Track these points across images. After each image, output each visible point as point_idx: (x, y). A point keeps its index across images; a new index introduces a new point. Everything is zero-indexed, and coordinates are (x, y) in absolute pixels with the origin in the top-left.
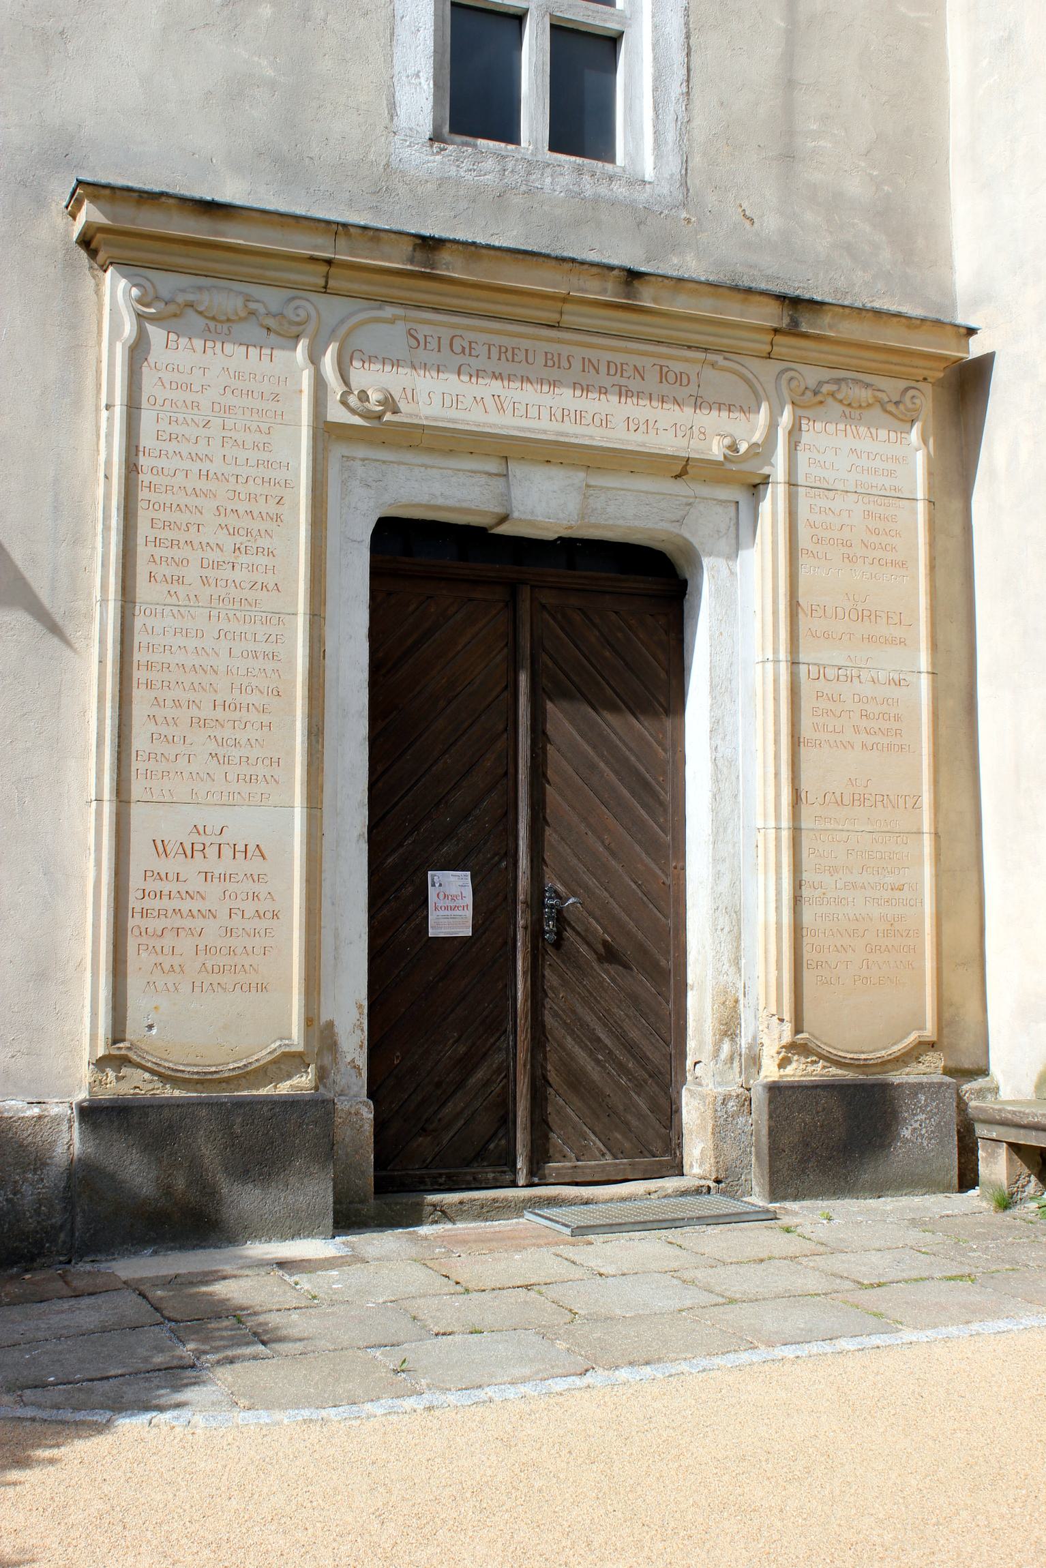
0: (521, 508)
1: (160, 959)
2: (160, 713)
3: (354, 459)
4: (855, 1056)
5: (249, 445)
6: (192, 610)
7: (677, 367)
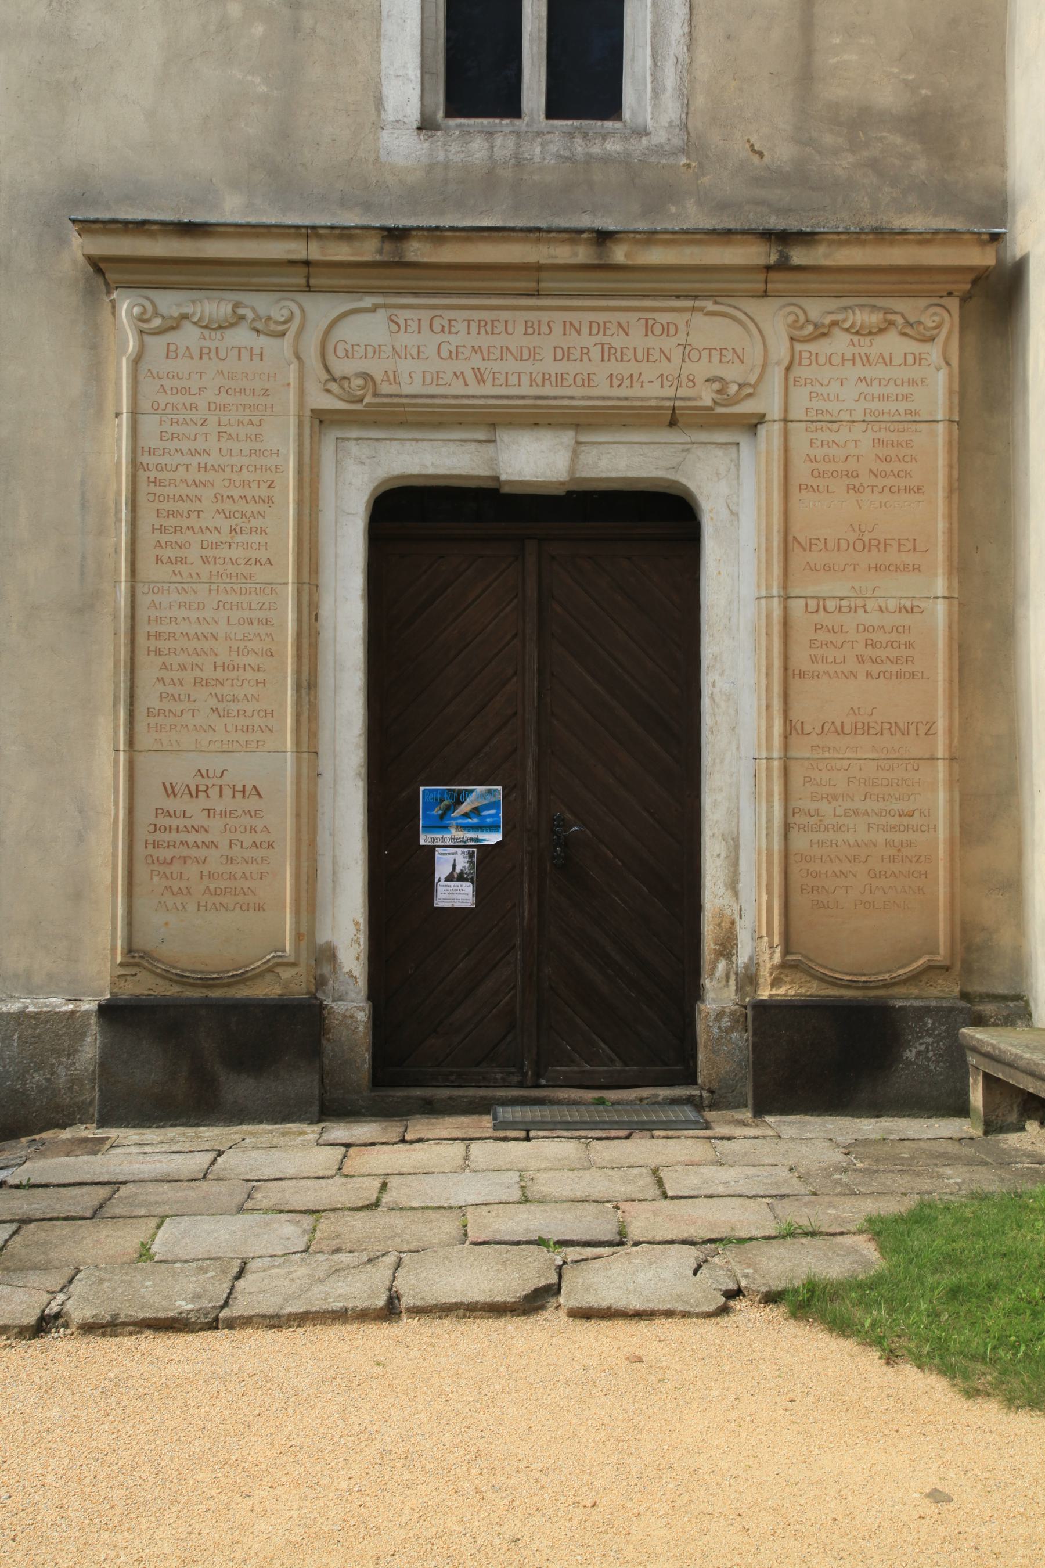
0: (509, 471)
1: (170, 883)
2: (167, 675)
3: (348, 439)
4: (854, 978)
5: (242, 437)
6: (194, 586)
7: (664, 318)
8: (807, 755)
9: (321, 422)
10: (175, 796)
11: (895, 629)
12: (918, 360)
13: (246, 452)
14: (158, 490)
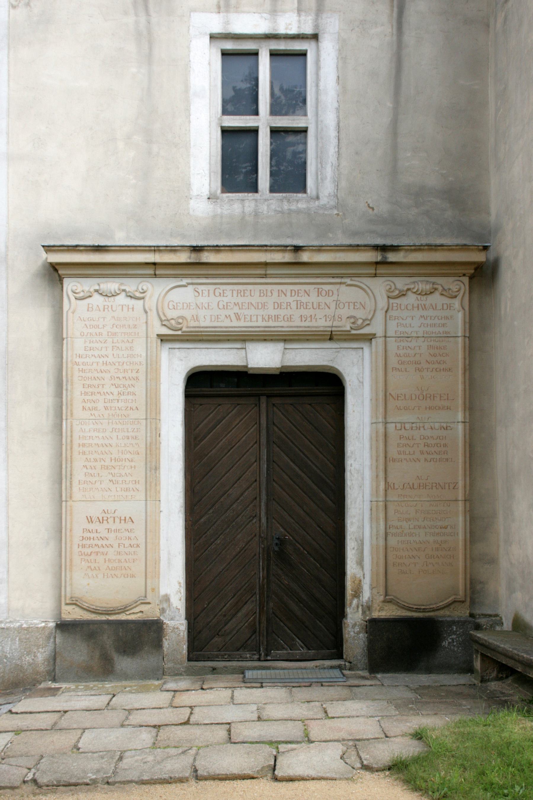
1: (90, 564)
2: (88, 464)
6: (101, 421)
8: (396, 499)
9: (162, 340)
10: (92, 522)
11: (439, 437)
12: (450, 307)
13: (125, 356)
14: (83, 375)
